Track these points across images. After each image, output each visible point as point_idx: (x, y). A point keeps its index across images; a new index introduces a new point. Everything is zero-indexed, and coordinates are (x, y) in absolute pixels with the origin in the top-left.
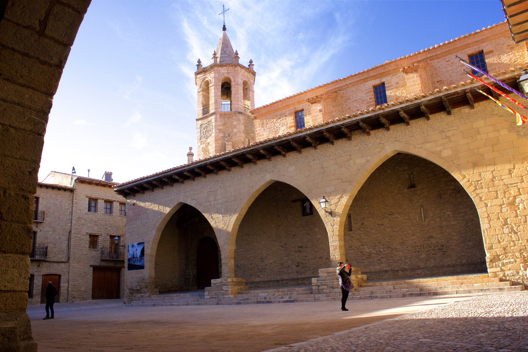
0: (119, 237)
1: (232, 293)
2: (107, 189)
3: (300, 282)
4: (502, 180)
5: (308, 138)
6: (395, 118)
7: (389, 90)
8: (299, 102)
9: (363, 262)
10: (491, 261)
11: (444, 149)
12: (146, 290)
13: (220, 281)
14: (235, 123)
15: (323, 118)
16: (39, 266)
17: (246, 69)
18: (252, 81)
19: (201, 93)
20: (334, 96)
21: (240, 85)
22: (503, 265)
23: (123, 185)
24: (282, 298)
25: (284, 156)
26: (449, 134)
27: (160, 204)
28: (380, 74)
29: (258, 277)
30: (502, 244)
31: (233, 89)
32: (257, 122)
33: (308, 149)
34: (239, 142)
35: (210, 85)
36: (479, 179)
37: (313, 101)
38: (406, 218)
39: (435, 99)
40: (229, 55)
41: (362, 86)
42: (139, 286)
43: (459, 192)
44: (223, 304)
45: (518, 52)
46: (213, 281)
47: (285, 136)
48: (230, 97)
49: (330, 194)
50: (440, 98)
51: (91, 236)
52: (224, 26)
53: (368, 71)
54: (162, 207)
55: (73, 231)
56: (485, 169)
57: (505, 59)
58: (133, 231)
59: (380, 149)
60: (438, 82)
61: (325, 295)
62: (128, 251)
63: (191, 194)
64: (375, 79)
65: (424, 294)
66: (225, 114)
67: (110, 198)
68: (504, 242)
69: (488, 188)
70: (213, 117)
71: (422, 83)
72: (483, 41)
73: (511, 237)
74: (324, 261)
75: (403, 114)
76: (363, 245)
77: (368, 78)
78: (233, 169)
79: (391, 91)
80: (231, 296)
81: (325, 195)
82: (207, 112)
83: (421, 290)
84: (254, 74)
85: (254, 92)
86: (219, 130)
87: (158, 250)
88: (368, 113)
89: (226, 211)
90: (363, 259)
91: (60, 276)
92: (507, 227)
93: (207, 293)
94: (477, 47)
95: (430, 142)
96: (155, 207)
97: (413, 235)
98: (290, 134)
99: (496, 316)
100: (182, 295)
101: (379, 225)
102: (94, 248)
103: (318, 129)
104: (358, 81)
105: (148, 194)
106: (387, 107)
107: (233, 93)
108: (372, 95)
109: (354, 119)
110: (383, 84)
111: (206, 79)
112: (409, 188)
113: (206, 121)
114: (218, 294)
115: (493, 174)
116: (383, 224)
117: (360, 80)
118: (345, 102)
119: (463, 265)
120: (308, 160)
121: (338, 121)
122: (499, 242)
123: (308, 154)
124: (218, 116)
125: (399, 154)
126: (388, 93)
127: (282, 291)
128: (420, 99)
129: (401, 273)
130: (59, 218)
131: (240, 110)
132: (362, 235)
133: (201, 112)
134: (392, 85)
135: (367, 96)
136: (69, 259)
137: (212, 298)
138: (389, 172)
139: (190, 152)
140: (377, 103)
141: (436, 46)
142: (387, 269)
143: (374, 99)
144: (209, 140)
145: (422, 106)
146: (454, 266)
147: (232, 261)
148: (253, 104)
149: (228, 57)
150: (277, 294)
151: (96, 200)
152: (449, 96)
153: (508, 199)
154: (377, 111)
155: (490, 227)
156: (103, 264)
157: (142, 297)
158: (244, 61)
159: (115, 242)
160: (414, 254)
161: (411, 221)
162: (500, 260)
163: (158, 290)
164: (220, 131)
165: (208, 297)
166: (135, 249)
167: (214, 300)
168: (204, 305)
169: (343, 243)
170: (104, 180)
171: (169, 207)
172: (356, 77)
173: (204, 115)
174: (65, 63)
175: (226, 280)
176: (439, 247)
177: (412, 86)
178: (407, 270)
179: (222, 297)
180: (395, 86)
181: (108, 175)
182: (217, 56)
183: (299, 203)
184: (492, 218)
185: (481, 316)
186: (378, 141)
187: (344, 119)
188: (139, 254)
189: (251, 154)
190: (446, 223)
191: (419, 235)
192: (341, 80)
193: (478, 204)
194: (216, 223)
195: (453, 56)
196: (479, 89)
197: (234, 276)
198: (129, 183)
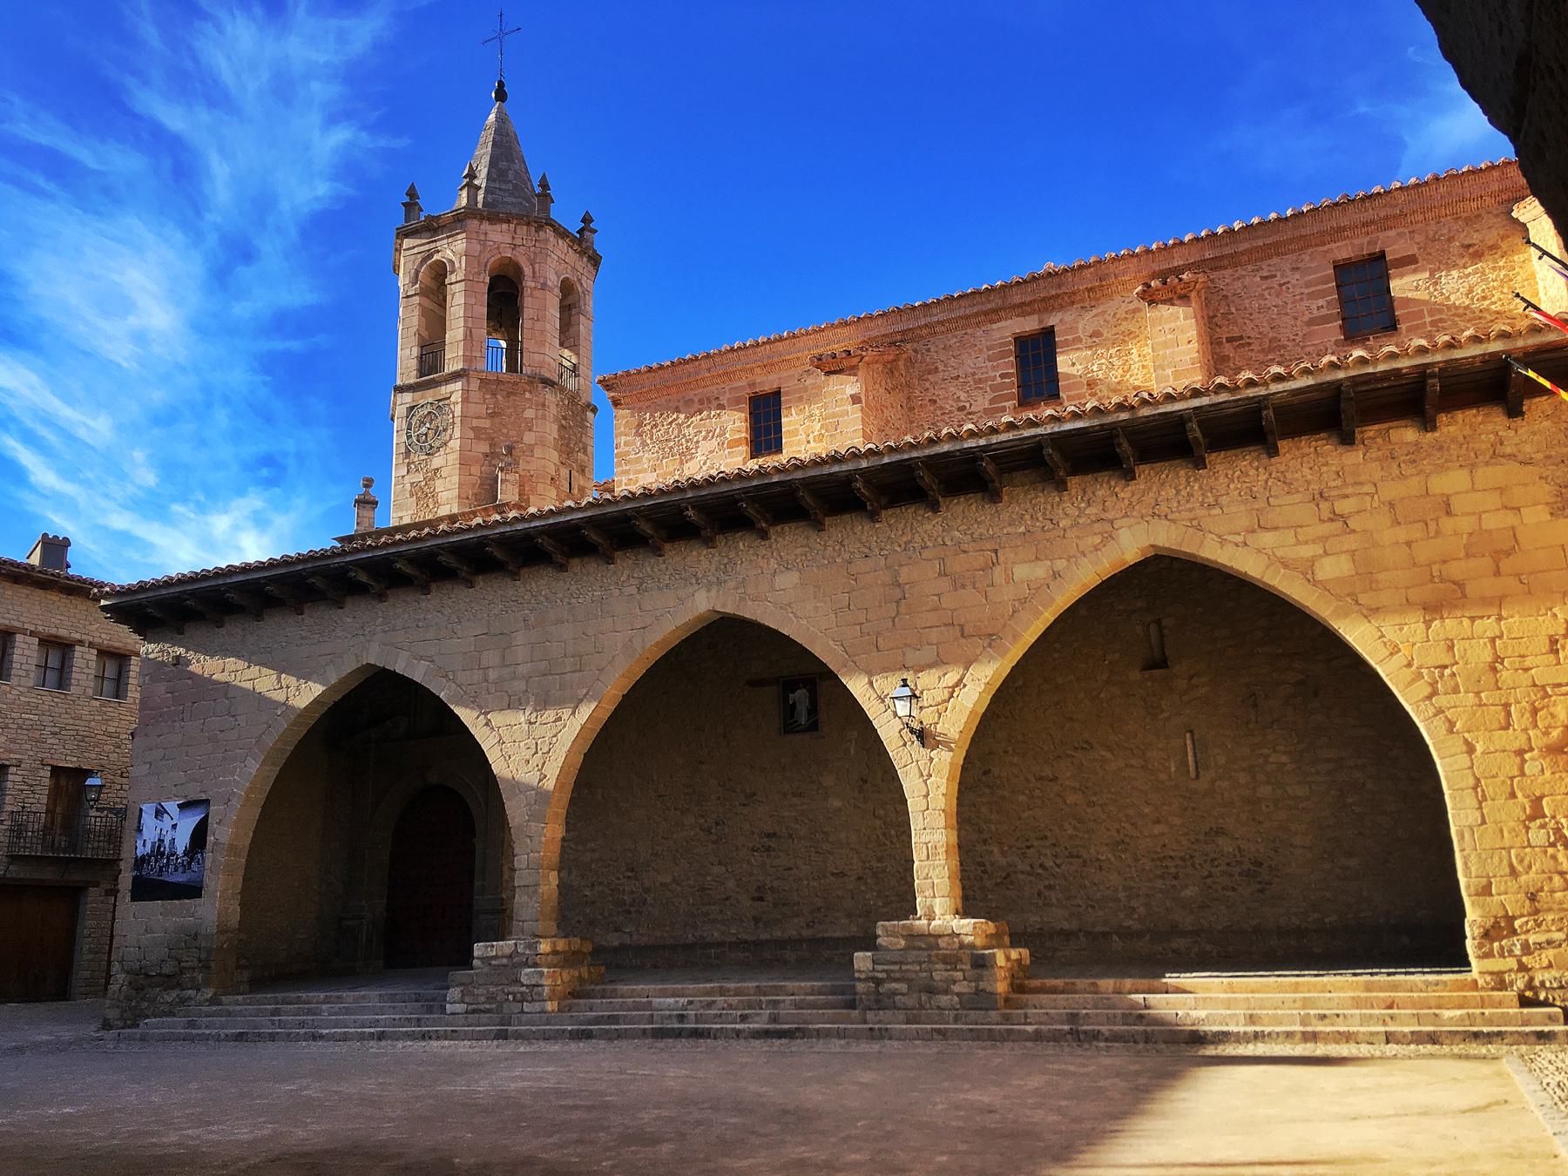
4: (1527, 670)
13: (508, 951)
14: (529, 413)
17: (574, 239)
22: (1526, 948)
24: (744, 1018)
25: (764, 535)
26: (1343, 507)
27: (281, 667)
28: (1043, 299)
29: (617, 930)
30: (1523, 878)
35: (452, 278)
36: (1447, 661)
38: (1133, 762)
40: (516, 187)
43: (1316, 694)
45: (1494, 269)
50: (1337, 385)
52: (501, 84)
57: (1456, 286)
60: (1229, 340)
61: (901, 1015)
62: (139, 830)
64: (1024, 314)
67: (63, 632)
68: (1532, 874)
69: (1478, 694)
70: (458, 385)
72: (1386, 223)
73: (1554, 857)
76: (985, 841)
77: (1003, 309)
78: (575, 563)
79: (1074, 356)
90: (983, 888)
92: (1543, 826)
94: (1365, 240)
95: (1276, 528)
96: (263, 681)
97: (1158, 822)
101: (1041, 778)
103: (896, 457)
104: (967, 317)
105: (234, 630)
108: (1009, 365)
109: (1027, 433)
110: (1049, 332)
112: (1145, 668)
113: (429, 396)
115: (1494, 647)
116: (1054, 779)
117: (977, 314)
120: (847, 556)
121: (972, 434)
122: (1513, 872)
124: (475, 384)
126: (1064, 363)
127: (738, 993)
131: (547, 375)
132: (984, 810)
133: (414, 363)
134: (1079, 340)
137: (474, 1011)
141: (1237, 226)
144: (437, 461)
145: (1266, 408)
147: (553, 878)
153: (1546, 733)
155: (1484, 822)
160: (1159, 884)
161: (1179, 779)
162: (1514, 932)
165: (460, 1008)
170: (35, 560)
172: (963, 303)
175: (532, 946)
179: (516, 1007)
181: (55, 548)
184: (1490, 792)
188: (182, 841)
190: (1269, 788)
191: (1178, 821)
192: (914, 308)
194: (501, 742)
196: (1527, 366)
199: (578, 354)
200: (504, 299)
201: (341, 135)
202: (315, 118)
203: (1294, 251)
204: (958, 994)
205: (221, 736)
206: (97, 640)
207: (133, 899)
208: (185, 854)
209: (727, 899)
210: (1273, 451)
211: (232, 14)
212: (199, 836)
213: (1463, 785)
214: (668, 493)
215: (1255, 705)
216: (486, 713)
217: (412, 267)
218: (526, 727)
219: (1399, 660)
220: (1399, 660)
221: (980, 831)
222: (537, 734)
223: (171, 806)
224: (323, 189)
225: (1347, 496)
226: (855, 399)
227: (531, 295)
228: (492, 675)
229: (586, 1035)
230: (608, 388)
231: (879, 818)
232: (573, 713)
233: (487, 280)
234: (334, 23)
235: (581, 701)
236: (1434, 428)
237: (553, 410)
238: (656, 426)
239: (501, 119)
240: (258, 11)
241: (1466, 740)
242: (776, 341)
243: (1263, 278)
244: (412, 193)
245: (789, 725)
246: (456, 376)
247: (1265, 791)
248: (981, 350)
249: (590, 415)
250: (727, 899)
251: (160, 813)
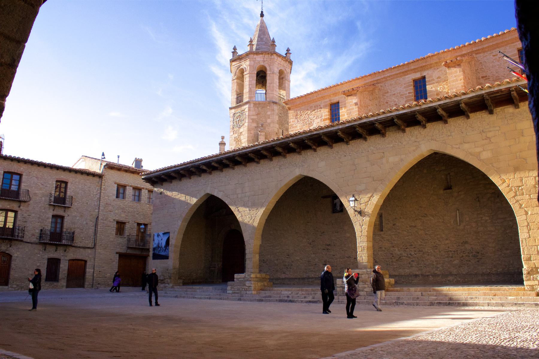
0: (146, 225)
1: (255, 290)
2: (136, 176)
5: (339, 133)
6: (433, 116)
7: (430, 84)
8: (335, 94)
9: (393, 265)
10: (528, 273)
11: (484, 150)
12: (169, 281)
14: (269, 113)
15: (359, 111)
16: (65, 251)
17: (283, 57)
18: (289, 70)
19: (236, 81)
20: (371, 89)
21: (276, 74)
23: (151, 173)
24: (305, 297)
25: (315, 150)
26: (490, 135)
27: (187, 194)
28: (421, 67)
29: (284, 273)
31: (268, 78)
32: (291, 113)
33: (339, 144)
34: (273, 134)
35: (245, 73)
37: (349, 94)
39: (476, 96)
40: (266, 43)
41: (401, 79)
42: (162, 277)
44: (245, 300)
46: (236, 276)
47: (316, 130)
48: (266, 86)
49: (360, 192)
50: (482, 95)
51: (118, 222)
52: (262, 12)
53: (408, 64)
54: (189, 197)
55: (100, 218)
56: (527, 174)
59: (414, 148)
60: (482, 77)
62: (154, 240)
63: (219, 185)
64: (415, 72)
65: (453, 303)
66: (259, 104)
67: (139, 186)
69: (530, 195)
70: (247, 106)
71: (465, 78)
74: (352, 261)
75: (440, 111)
76: (393, 247)
77: (408, 71)
78: (262, 161)
79: (432, 86)
80: (253, 292)
81: (354, 193)
82: (241, 101)
83: (451, 299)
84: (291, 63)
85: (289, 81)
86: (253, 120)
87: (183, 240)
88: (403, 109)
89: (253, 205)
90: (392, 262)
91: (86, 262)
93: (230, 287)
95: (469, 143)
96: (182, 197)
97: (447, 240)
98: (322, 128)
99: (519, 346)
100: (205, 288)
101: (411, 226)
102: (121, 234)
104: (397, 74)
105: (175, 183)
106: (424, 103)
107: (268, 82)
108: (411, 89)
109: (389, 115)
110: (424, 78)
111: (241, 67)
112: (445, 189)
113: (239, 110)
114: (241, 289)
116: (415, 226)
117: (400, 73)
118: (383, 95)
119: (498, 274)
121: (372, 116)
123: (340, 149)
124: (252, 105)
125: (436, 153)
126: (428, 88)
127: (306, 291)
128: (460, 96)
129: (431, 278)
130: (87, 203)
131: (274, 100)
132: (393, 236)
133: (235, 100)
134: (433, 80)
135: (406, 91)
136: (95, 245)
137: (234, 293)
138: (425, 171)
139: (222, 141)
140: (417, 99)
142: (417, 273)
143: (413, 94)
144: (241, 130)
145: (461, 104)
146: (489, 274)
147: (257, 257)
148: (288, 94)
149: (264, 45)
150: (300, 292)
151: (124, 187)
152: (492, 94)
154: (413, 107)
155: (530, 237)
156: (129, 251)
157: (165, 287)
158: (281, 49)
159: (143, 229)
161: (445, 224)
163: (181, 281)
164: (253, 120)
165: (230, 292)
166: (160, 238)
167: (236, 295)
168: (226, 299)
169: (371, 244)
170: (134, 166)
171: (196, 197)
172: (395, 70)
173: (237, 103)
174: (19, 62)
175: (249, 275)
176: (474, 253)
177: (453, 81)
178: (438, 276)
179: (245, 292)
180: (436, 80)
181: (138, 162)
182: (253, 43)
183: (329, 199)
184: (532, 227)
185: (502, 344)
186: (413, 139)
187: (379, 115)
188: (164, 244)
189: (280, 147)
191: (453, 239)
192: (379, 72)
193: (518, 211)
194: (242, 216)
195: (496, 52)
196: (525, 88)
197: (258, 272)
198: (157, 171)
203: (503, 46)
204: (366, 292)
210: (468, 117)
213: (524, 225)
215: (479, 201)
219: (505, 185)
220: (505, 185)
221: (392, 243)
225: (491, 131)
226: (356, 104)
228: (240, 196)
229: (261, 300)
236: (518, 108)
237: (277, 111)
241: (525, 210)
243: (494, 56)
246: (247, 103)
247: (481, 229)
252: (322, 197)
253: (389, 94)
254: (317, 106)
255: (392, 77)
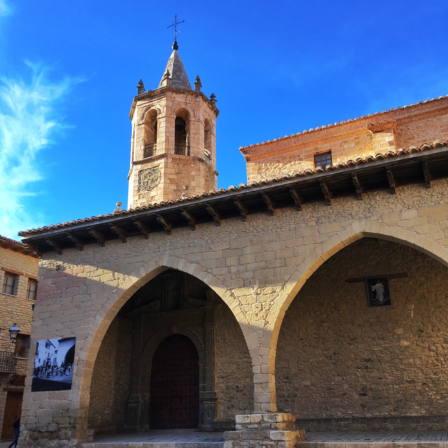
3: (376, 425)
12: (70, 433)
13: (258, 420)
14: (193, 173)
27: (115, 270)
40: (184, 82)
52: (176, 43)
58: (50, 317)
62: (37, 354)
70: (163, 160)
74: (419, 388)
86: (171, 180)
96: (105, 276)
105: (90, 251)
111: (152, 108)
113: (149, 165)
117: (435, 111)
124: (170, 160)
131: (200, 157)
133: (142, 152)
163: (92, 431)
166: (52, 350)
172: (428, 105)
188: (61, 359)
194: (240, 304)
199: (210, 151)
200: (181, 125)
201: (50, 125)
202: (42, 118)
205: (82, 305)
206: (5, 267)
207: (33, 390)
208: (62, 366)
209: (344, 395)
211: (13, 84)
212: (70, 357)
214: (346, 166)
216: (231, 290)
217: (141, 112)
218: (254, 296)
222: (262, 300)
223: (55, 341)
224: (44, 142)
227: (193, 124)
228: (233, 269)
230: (245, 152)
231: (433, 351)
232: (283, 288)
233: (175, 117)
234: (49, 88)
235: (287, 282)
237: (203, 173)
238: (268, 169)
239: (176, 56)
240: (23, 83)
242: (331, 127)
244: (141, 83)
245: (372, 300)
246: (161, 157)
248: (437, 128)
249: (216, 176)
250: (344, 395)
251: (48, 345)
252: (347, 281)
253: (416, 140)
254: (294, 157)
255: (420, 117)
